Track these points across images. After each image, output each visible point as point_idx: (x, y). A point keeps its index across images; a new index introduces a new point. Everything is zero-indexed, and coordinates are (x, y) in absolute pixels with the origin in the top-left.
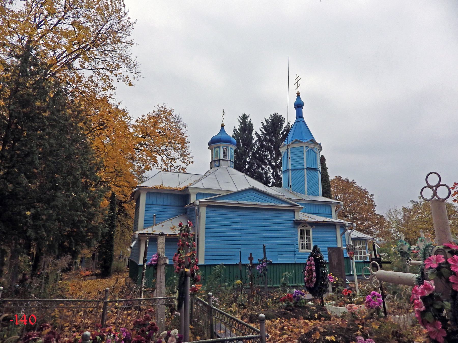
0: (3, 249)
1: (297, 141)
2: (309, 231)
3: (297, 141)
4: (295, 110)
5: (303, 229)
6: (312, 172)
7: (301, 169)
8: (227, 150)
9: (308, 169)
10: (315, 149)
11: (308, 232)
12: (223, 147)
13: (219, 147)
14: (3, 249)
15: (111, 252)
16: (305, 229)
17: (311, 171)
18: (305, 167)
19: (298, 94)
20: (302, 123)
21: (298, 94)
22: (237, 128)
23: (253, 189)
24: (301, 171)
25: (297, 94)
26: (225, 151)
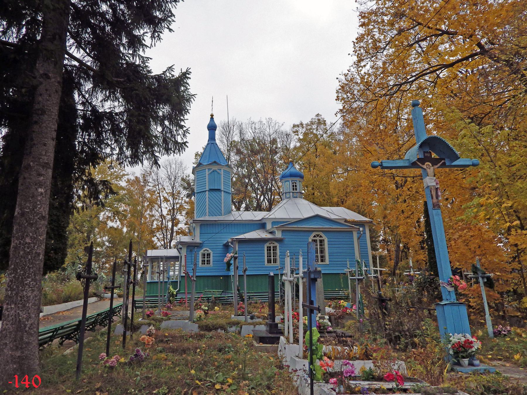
0: (479, 341)
1: (215, 162)
2: (276, 247)
3: (215, 162)
4: (208, 132)
5: (270, 245)
6: (214, 194)
7: (203, 191)
8: (296, 183)
9: (211, 190)
10: (218, 171)
11: (275, 248)
12: (292, 181)
13: (296, 181)
14: (479, 341)
15: (103, 326)
16: (272, 245)
17: (215, 192)
18: (207, 189)
19: (212, 116)
20: (215, 144)
21: (212, 116)
22: (158, 161)
23: (317, 217)
24: (203, 193)
25: (211, 115)
26: (294, 184)
